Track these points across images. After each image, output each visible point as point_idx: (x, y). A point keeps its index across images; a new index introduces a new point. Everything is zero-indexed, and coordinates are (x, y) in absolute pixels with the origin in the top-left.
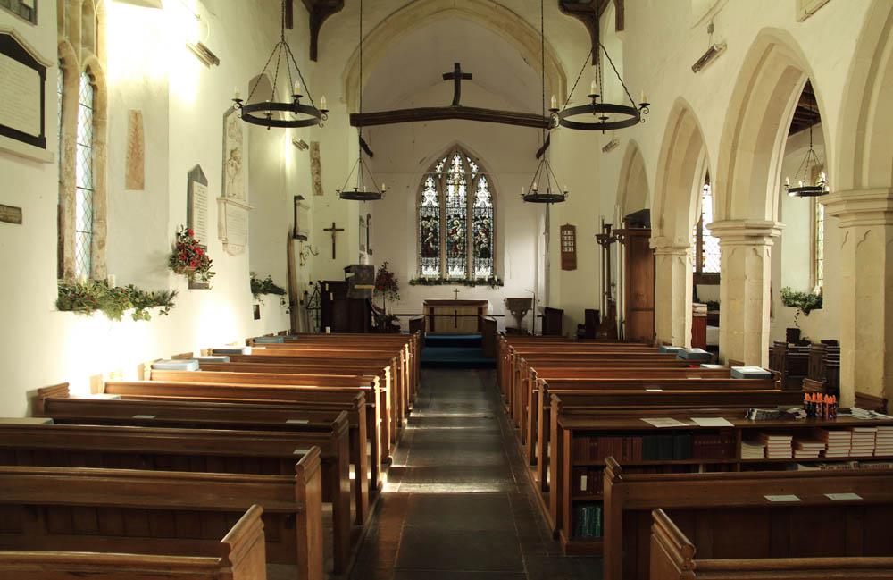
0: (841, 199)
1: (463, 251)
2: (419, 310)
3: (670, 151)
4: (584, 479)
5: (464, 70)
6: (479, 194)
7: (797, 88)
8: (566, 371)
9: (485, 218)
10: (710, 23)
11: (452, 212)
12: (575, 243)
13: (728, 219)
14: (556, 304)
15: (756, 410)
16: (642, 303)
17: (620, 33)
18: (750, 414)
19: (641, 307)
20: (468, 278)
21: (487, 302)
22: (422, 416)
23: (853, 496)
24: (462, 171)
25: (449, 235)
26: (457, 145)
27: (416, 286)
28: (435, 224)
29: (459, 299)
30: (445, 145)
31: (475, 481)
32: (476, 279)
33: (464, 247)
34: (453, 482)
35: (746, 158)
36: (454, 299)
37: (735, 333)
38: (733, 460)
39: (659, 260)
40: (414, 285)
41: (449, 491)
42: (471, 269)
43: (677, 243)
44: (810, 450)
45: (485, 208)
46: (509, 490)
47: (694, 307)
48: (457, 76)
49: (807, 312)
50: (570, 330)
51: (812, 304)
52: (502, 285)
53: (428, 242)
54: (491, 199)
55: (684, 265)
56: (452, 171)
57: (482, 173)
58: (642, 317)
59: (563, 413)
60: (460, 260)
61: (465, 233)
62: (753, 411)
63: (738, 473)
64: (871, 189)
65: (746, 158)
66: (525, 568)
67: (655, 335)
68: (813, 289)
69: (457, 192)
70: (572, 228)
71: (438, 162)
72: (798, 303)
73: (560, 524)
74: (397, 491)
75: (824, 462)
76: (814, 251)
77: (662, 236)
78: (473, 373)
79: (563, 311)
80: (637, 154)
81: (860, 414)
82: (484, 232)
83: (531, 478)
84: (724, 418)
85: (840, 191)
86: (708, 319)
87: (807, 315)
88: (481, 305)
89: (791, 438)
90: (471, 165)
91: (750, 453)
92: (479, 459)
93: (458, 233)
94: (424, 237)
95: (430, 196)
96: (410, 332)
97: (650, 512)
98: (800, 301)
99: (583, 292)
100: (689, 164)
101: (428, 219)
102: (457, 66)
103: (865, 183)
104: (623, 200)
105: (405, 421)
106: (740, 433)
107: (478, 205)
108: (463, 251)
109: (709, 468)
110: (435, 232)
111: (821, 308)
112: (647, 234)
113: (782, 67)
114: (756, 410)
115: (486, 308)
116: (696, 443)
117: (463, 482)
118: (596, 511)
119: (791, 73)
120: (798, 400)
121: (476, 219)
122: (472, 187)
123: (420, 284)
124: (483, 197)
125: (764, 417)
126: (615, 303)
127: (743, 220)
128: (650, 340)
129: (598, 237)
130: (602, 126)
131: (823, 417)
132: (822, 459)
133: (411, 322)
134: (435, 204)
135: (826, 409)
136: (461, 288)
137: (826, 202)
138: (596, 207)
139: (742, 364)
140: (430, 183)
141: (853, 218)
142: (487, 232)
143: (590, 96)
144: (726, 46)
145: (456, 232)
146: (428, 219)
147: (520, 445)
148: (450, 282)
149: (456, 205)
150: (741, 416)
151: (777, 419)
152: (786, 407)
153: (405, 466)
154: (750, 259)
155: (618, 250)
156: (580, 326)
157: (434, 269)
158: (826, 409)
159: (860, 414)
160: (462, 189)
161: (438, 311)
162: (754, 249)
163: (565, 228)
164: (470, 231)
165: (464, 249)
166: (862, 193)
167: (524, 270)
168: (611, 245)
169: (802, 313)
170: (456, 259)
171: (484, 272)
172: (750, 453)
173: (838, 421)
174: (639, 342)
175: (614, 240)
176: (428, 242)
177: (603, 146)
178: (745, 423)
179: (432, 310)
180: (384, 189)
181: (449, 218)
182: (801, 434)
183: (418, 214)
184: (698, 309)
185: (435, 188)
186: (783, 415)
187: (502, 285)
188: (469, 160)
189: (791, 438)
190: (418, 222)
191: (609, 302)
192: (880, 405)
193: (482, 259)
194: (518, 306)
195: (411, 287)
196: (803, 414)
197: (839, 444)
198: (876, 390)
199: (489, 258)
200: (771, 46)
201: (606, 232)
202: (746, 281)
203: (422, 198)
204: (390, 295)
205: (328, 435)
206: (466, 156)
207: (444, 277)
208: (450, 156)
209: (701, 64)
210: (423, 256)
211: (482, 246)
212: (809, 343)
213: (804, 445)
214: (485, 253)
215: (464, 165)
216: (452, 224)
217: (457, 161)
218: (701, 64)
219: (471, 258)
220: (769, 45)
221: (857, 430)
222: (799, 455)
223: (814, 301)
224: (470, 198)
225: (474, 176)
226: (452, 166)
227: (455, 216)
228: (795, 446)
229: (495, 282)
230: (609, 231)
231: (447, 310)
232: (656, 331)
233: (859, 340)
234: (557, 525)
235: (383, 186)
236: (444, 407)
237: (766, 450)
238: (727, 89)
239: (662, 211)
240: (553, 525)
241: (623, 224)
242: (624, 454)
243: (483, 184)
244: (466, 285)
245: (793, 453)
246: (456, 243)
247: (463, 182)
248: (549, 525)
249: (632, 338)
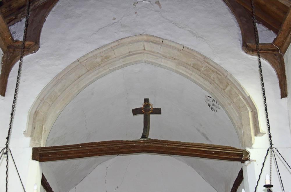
5: (154, 104)
48: (146, 110)
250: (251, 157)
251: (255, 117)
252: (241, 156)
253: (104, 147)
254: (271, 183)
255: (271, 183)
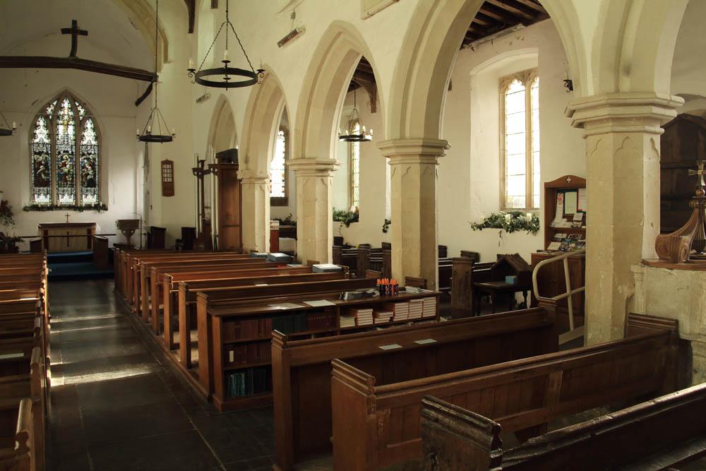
0: (392, 145)
1: (72, 181)
2: (35, 232)
3: (255, 104)
4: (232, 353)
5: (81, 27)
6: (85, 134)
7: (354, 65)
8: (187, 275)
9: (91, 153)
10: (292, 12)
11: (62, 148)
12: (173, 175)
13: (303, 158)
14: (158, 223)
15: (347, 293)
16: (232, 219)
17: (214, 10)
18: (343, 296)
19: (231, 224)
20: (52, 202)
21: (94, 224)
22: (60, 321)
23: (431, 341)
24: (71, 113)
25: (59, 168)
26: (67, 90)
27: (30, 212)
28: (46, 158)
29: (70, 222)
30: (58, 89)
31: (128, 367)
32: (84, 205)
33: (73, 177)
34: (109, 370)
35: (317, 113)
36: (64, 222)
37: (309, 240)
38: (335, 329)
39: (245, 188)
40: (27, 211)
41: (109, 378)
42: (79, 196)
43: (259, 175)
44: (384, 317)
45: (91, 145)
46: (159, 371)
47: (271, 223)
48: (74, 31)
49: (348, 225)
50: (170, 243)
51: (350, 219)
52: (107, 210)
53: (40, 174)
54: (97, 138)
55: (264, 191)
56: (62, 113)
57: (89, 115)
58: (232, 232)
59: (210, 306)
60: (69, 189)
61: (73, 166)
62: (344, 293)
63: (339, 336)
64: (412, 139)
65: (317, 113)
66: (194, 426)
67: (241, 245)
68: (350, 208)
69: (66, 131)
70: (170, 163)
71: (49, 105)
72: (341, 218)
73: (212, 389)
74: (63, 384)
75: (393, 324)
76: (351, 181)
77: (247, 169)
78: (91, 283)
79: (165, 229)
80: (226, 105)
81: (411, 290)
82: (90, 165)
83: (174, 361)
84: (326, 300)
85: (391, 140)
86: (287, 229)
87: (348, 227)
88: (90, 227)
89: (372, 310)
90: (79, 108)
91: (346, 323)
92: (112, 351)
93: (68, 166)
94: (36, 170)
95: (42, 134)
96: (30, 251)
97: (330, 362)
98: (343, 216)
99: (181, 213)
100: (268, 117)
101: (40, 153)
102: (74, 22)
103: (408, 134)
104: (213, 140)
105: (49, 326)
106: (339, 310)
107: (85, 143)
108: (72, 181)
109: (317, 335)
110: (46, 165)
111: (357, 221)
112: (236, 167)
113: (346, 49)
114: (347, 293)
115: (94, 229)
116: (309, 319)
117: (118, 370)
118: (241, 377)
119: (352, 53)
120: (372, 283)
121: (83, 155)
122: (80, 127)
123: (34, 210)
124: (89, 136)
125: (353, 297)
126: (210, 221)
127: (315, 158)
128: (240, 250)
129: (194, 170)
130: (226, 85)
131: (390, 295)
132: (392, 322)
133: (32, 243)
134: (46, 141)
135: (392, 289)
136: (71, 212)
137: (381, 147)
138: (195, 145)
139: (318, 263)
140: (41, 122)
141: (400, 158)
142: (93, 166)
143: (224, 62)
144: (305, 30)
145: (66, 165)
146: (40, 153)
147: (155, 336)
148: (63, 207)
149: (66, 143)
150: (336, 298)
151: (362, 297)
152: (365, 289)
153: (62, 363)
154: (319, 187)
155: (212, 181)
156: (178, 241)
157: (46, 197)
158: (392, 289)
159: (411, 290)
160: (71, 129)
161: (51, 232)
162: (322, 180)
163: (164, 163)
164: (78, 165)
165: (73, 179)
166: (406, 141)
167: (124, 198)
168: (205, 176)
169: (344, 225)
170: (66, 188)
171: (90, 199)
172: (346, 323)
173: (399, 296)
174: (229, 251)
175: (208, 172)
176: (40, 174)
177: (198, 98)
178: (340, 302)
179: (46, 233)
180: (14, 127)
181: (59, 153)
182: (378, 307)
183: (30, 149)
184: (273, 225)
185: (46, 127)
186: (365, 295)
187: (107, 210)
188: (77, 104)
189: (372, 310)
190: (30, 156)
191: (203, 221)
192: (423, 284)
193: (89, 188)
194: (127, 226)
195: (24, 212)
196: (378, 293)
197: (402, 312)
198: (416, 274)
199: (95, 187)
200: (340, 34)
201: (200, 166)
202: (317, 203)
203: (34, 136)
204: (4, 220)
205: (29, 339)
206: (75, 101)
207: (55, 204)
208: (60, 99)
209: (284, 41)
210: (36, 186)
211: (89, 177)
212: (350, 247)
213: (381, 314)
214: (91, 183)
215: (73, 108)
216: (62, 159)
217: (66, 104)
218: (284, 41)
219: (79, 187)
220: (338, 32)
221: (412, 301)
222: (378, 321)
223: (352, 216)
224: (79, 137)
225: (81, 118)
226: (61, 108)
227: (64, 151)
228: (375, 316)
229: (100, 207)
230: (203, 166)
231: (64, 232)
232: (244, 242)
233: (405, 242)
234: (210, 392)
235: (14, 124)
236: (81, 312)
237: (356, 320)
238: (305, 63)
239: (248, 150)
240: (206, 392)
241: (216, 160)
242: (260, 332)
243: (89, 124)
244: (75, 210)
245: (374, 320)
246: (66, 174)
247: (71, 122)
248: (201, 392)
249: (224, 248)
250: (159, 79)
251: (588, 417)
252: (152, 78)
253: (360, 79)
254: (147, 148)
255: (147, 148)
